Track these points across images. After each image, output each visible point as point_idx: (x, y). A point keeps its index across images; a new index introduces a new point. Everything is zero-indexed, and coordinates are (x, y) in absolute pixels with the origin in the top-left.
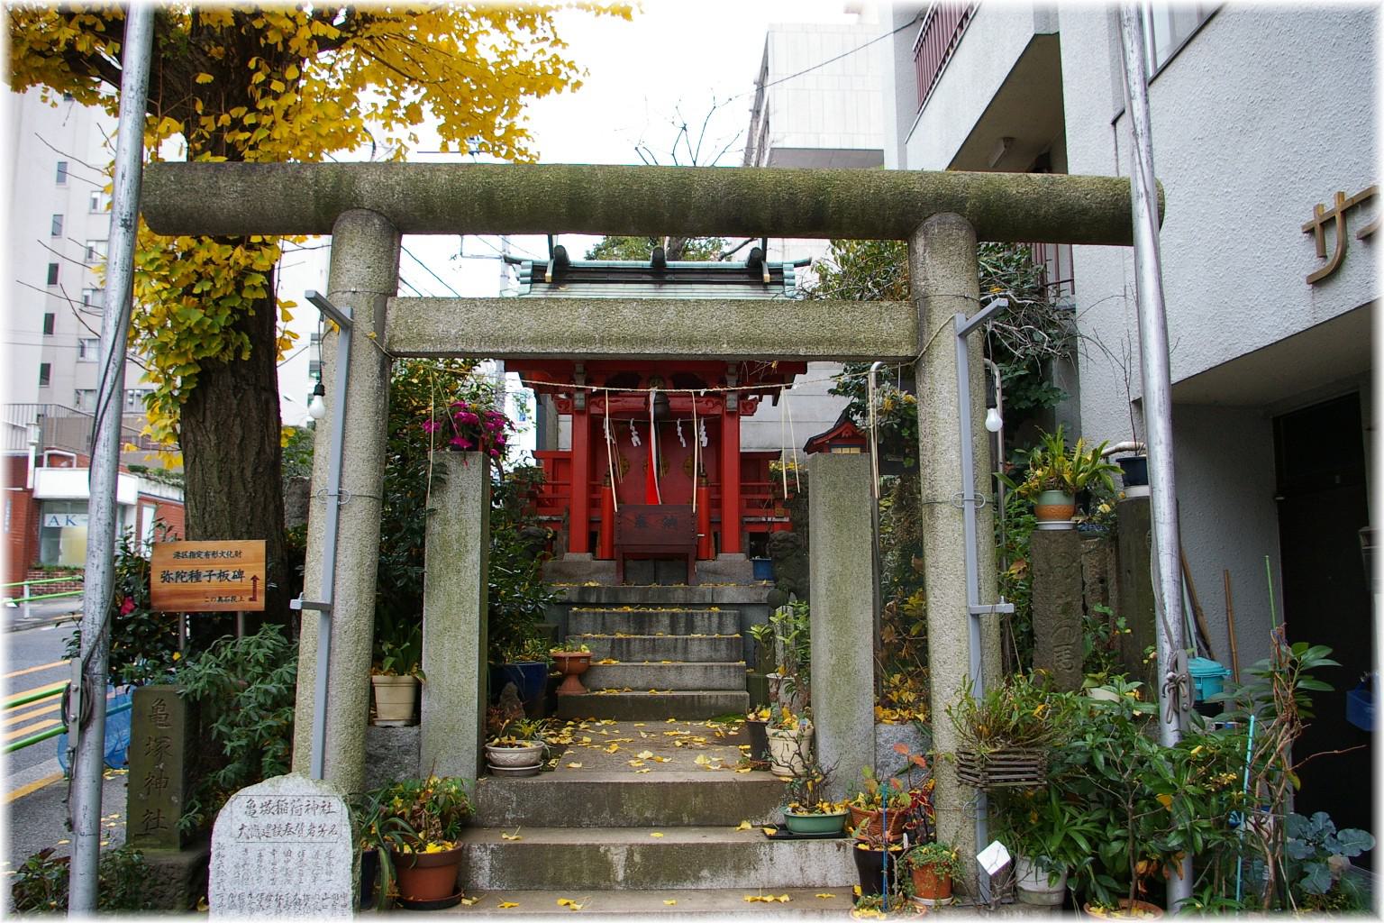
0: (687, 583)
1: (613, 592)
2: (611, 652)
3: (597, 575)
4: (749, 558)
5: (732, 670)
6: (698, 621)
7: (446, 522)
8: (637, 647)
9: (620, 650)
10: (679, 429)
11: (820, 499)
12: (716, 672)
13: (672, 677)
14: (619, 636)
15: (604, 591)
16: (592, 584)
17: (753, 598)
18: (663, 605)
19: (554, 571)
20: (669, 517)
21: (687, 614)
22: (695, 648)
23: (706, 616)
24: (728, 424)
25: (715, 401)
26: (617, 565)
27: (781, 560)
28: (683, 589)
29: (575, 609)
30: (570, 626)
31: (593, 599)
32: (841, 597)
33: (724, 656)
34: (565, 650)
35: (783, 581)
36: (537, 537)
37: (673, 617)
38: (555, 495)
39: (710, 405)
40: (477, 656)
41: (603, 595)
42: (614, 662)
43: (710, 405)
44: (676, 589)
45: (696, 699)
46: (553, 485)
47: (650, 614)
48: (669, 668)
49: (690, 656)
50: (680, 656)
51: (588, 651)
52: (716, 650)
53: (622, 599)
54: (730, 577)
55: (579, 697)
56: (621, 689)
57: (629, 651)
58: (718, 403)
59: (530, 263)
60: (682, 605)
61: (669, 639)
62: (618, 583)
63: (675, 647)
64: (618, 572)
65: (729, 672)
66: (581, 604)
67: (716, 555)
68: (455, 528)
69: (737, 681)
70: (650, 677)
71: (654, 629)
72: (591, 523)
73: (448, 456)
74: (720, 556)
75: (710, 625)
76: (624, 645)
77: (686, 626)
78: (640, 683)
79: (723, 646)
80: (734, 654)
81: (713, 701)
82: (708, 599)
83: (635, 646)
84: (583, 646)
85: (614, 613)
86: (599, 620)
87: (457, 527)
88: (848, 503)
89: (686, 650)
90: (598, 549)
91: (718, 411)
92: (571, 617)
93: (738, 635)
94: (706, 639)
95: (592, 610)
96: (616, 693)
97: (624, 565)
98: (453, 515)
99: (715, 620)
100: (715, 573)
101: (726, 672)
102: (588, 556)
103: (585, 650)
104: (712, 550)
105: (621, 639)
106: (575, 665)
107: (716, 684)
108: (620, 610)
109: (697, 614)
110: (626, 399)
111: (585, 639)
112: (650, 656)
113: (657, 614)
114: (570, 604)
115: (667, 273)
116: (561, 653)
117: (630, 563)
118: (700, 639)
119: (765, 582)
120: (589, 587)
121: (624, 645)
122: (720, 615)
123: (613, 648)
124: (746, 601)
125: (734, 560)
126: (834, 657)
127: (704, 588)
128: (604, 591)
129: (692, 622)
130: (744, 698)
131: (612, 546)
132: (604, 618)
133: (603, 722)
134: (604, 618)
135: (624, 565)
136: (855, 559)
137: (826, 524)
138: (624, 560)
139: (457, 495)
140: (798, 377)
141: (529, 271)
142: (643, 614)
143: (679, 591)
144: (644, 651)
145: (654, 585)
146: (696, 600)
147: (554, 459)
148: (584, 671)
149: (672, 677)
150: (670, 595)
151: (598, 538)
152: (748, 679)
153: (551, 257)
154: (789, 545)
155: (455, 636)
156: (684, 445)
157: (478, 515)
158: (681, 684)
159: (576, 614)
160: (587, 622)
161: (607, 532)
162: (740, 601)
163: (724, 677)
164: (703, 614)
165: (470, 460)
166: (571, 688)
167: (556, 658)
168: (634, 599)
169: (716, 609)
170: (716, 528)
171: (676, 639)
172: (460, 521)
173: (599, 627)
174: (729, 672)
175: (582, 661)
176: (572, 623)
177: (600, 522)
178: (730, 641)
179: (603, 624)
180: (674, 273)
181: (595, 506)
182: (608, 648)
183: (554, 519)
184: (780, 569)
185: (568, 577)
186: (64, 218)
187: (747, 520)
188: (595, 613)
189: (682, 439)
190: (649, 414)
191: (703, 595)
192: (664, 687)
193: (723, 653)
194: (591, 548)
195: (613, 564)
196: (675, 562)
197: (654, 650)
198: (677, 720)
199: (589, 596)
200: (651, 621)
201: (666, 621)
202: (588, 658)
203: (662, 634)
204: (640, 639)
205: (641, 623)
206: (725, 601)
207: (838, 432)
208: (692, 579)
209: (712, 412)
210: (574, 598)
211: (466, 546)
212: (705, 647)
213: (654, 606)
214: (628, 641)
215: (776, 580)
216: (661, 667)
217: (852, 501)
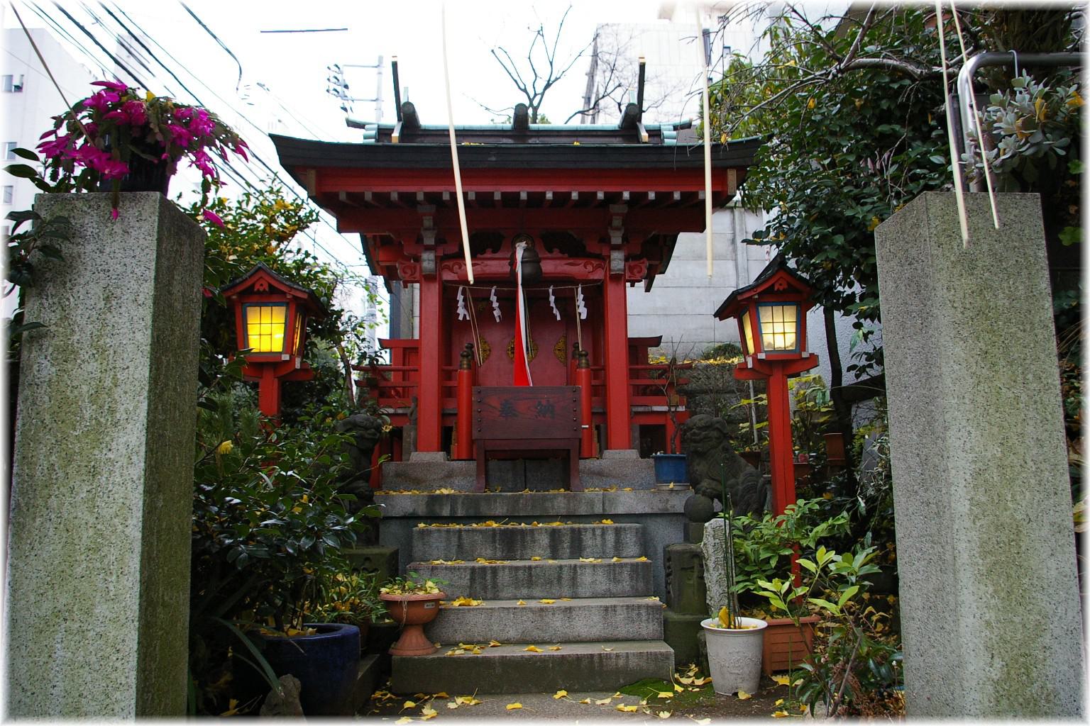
0: (568, 488)
1: (471, 501)
2: (471, 587)
3: (454, 481)
4: (644, 454)
5: (643, 612)
6: (588, 540)
7: (67, 354)
8: (507, 578)
9: (483, 584)
10: (552, 298)
11: (941, 293)
12: (621, 616)
13: (558, 624)
14: (482, 562)
15: (460, 501)
16: (445, 491)
17: (657, 506)
18: (540, 518)
19: (398, 475)
20: (544, 403)
21: (573, 530)
22: (586, 578)
23: (598, 532)
24: (611, 290)
25: (595, 263)
26: (478, 465)
27: (701, 455)
28: (565, 496)
29: (422, 525)
30: (415, 549)
31: (446, 512)
32: (1005, 518)
33: (628, 588)
34: (403, 590)
35: (705, 484)
36: (366, 428)
37: (554, 534)
38: (406, 383)
39: (590, 268)
40: (133, 681)
41: (459, 506)
42: (474, 603)
43: (590, 268)
44: (555, 496)
45: (596, 659)
46: (404, 371)
47: (522, 531)
48: (554, 611)
49: (581, 591)
50: (566, 590)
51: (436, 591)
52: (616, 581)
53: (485, 510)
54: (622, 480)
55: (422, 661)
56: (484, 643)
57: (495, 585)
58: (599, 266)
59: (376, 126)
60: (565, 518)
61: (550, 567)
62: (480, 489)
63: (560, 578)
64: (478, 475)
65: (639, 614)
66: (431, 518)
67: (601, 452)
68: (87, 369)
69: (649, 627)
70: (527, 625)
71: (529, 551)
72: (444, 415)
73: (79, 204)
74: (607, 453)
75: (604, 545)
76: (489, 577)
77: (572, 547)
78: (512, 633)
79: (626, 575)
80: (641, 585)
81: (621, 662)
82: (598, 509)
83: (504, 578)
84: (430, 584)
85: (474, 530)
86: (454, 540)
87: (93, 366)
88: (1002, 302)
89: (574, 582)
90: (454, 447)
91: (599, 275)
92: (416, 537)
93: (644, 559)
94: (601, 566)
95: (445, 527)
96: (477, 652)
97: (486, 466)
98: (86, 339)
99: (611, 538)
100: (600, 474)
101: (634, 614)
102: (440, 456)
103: (432, 589)
104: (596, 445)
105: (483, 569)
106: (417, 612)
107: (622, 631)
108: (482, 526)
109: (586, 529)
110: (486, 262)
111: (434, 568)
112: (525, 591)
113: (532, 531)
114: (413, 518)
115: (532, 136)
116: (397, 594)
117: (493, 464)
118: (594, 566)
119: (672, 485)
120: (442, 496)
121: (489, 577)
122: (618, 531)
123: (472, 580)
124: (648, 510)
125: (622, 457)
126: (998, 663)
127: (592, 494)
128: (460, 501)
129: (580, 541)
130: (666, 656)
131: (472, 442)
132: (460, 538)
133: (460, 700)
134: (460, 538)
135: (486, 466)
136: (1029, 429)
137: (959, 350)
138: (487, 460)
139: (96, 290)
140: (685, 240)
141: (373, 133)
142: (513, 531)
143: (558, 499)
144: (517, 584)
145: (527, 492)
146: (583, 510)
147: (405, 349)
148: (432, 620)
149: (558, 624)
150: (548, 504)
151: (454, 433)
152: (666, 623)
153: (399, 120)
154: (715, 434)
155: (81, 632)
156: (559, 318)
157: (144, 338)
158: (572, 633)
159: (422, 532)
160: (437, 543)
161: (464, 428)
162: (640, 509)
163: (633, 621)
164: (594, 529)
165: (130, 212)
166: (412, 646)
167: (390, 604)
168: (500, 510)
169: (608, 522)
170: (601, 418)
171: (561, 567)
172: (101, 351)
173: (454, 549)
174: (639, 614)
175: (427, 606)
176: (418, 547)
177: (456, 414)
178: (635, 567)
179: (460, 546)
180: (538, 136)
181: (450, 396)
182: (465, 582)
183: (400, 411)
184: (700, 467)
185: (416, 482)
186: (14, 189)
187: (635, 409)
188: (448, 531)
189: (555, 311)
190: (516, 275)
191: (591, 503)
192: (547, 638)
193: (626, 585)
194: (445, 445)
195: (473, 465)
196: (554, 462)
197: (530, 583)
198: (569, 690)
199: (441, 509)
200: (523, 541)
201: (544, 540)
202: (436, 601)
203: (539, 559)
204: (511, 568)
205: (511, 544)
206: (621, 510)
207: (769, 284)
208: (574, 482)
209: (591, 277)
210: (422, 510)
211: (112, 411)
212: (601, 576)
213: (528, 519)
214: (495, 570)
215: (694, 483)
216: (542, 609)
217: (1012, 298)
